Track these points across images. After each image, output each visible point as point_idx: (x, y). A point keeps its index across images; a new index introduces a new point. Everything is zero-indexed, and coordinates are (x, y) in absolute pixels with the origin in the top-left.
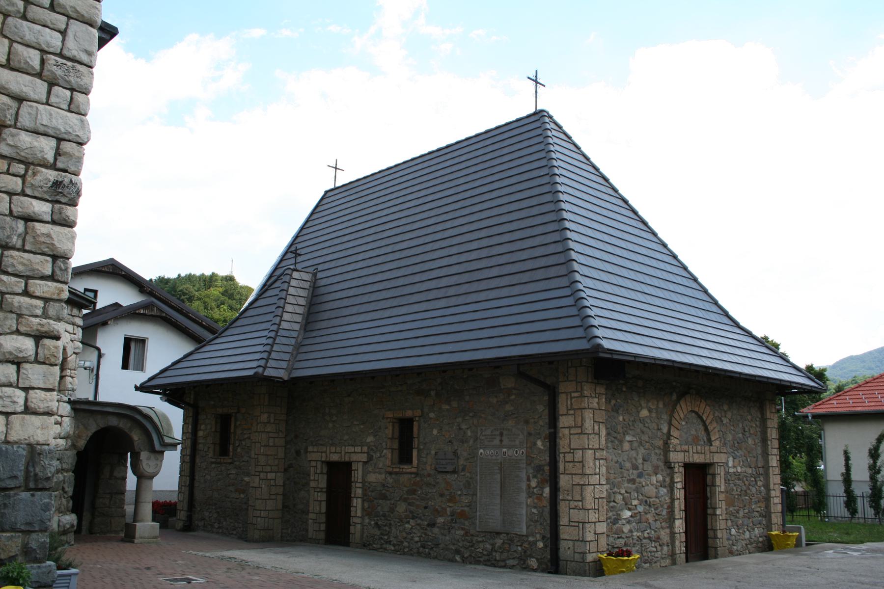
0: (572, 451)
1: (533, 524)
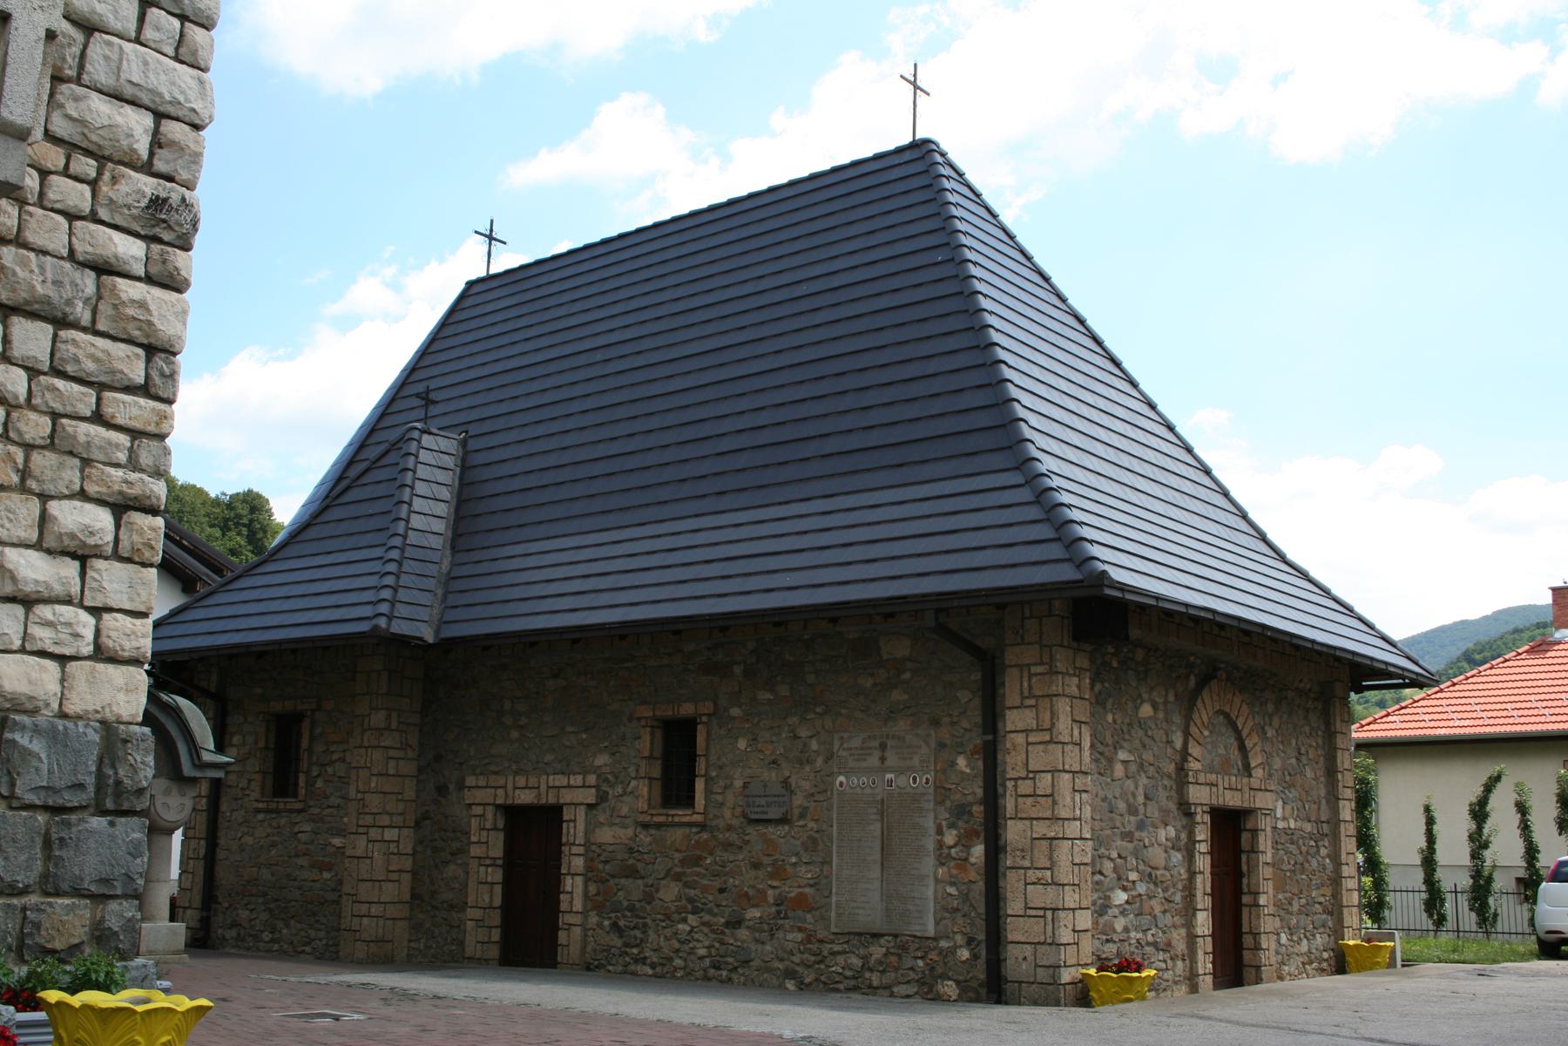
0: (1032, 775)
1: (948, 915)
